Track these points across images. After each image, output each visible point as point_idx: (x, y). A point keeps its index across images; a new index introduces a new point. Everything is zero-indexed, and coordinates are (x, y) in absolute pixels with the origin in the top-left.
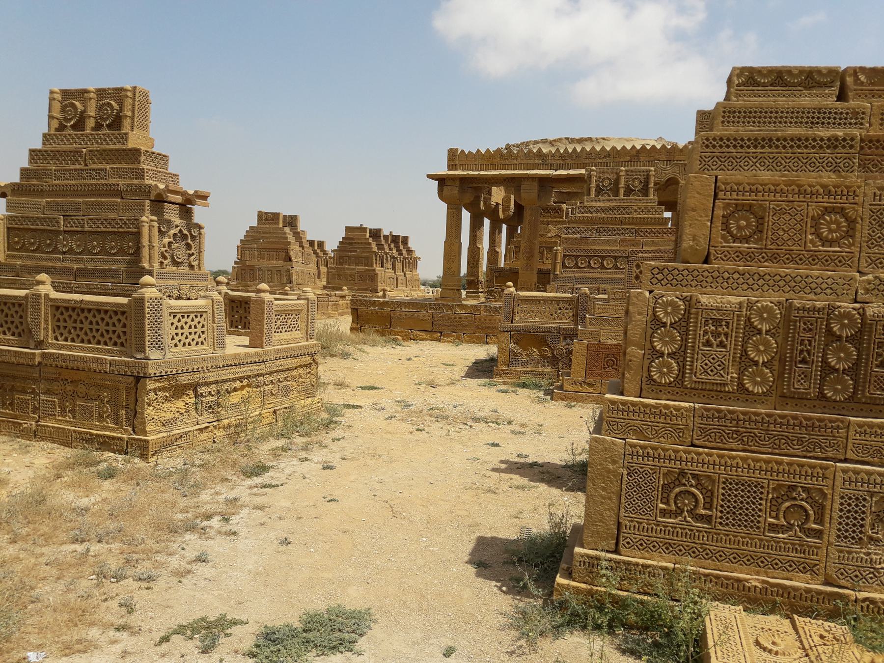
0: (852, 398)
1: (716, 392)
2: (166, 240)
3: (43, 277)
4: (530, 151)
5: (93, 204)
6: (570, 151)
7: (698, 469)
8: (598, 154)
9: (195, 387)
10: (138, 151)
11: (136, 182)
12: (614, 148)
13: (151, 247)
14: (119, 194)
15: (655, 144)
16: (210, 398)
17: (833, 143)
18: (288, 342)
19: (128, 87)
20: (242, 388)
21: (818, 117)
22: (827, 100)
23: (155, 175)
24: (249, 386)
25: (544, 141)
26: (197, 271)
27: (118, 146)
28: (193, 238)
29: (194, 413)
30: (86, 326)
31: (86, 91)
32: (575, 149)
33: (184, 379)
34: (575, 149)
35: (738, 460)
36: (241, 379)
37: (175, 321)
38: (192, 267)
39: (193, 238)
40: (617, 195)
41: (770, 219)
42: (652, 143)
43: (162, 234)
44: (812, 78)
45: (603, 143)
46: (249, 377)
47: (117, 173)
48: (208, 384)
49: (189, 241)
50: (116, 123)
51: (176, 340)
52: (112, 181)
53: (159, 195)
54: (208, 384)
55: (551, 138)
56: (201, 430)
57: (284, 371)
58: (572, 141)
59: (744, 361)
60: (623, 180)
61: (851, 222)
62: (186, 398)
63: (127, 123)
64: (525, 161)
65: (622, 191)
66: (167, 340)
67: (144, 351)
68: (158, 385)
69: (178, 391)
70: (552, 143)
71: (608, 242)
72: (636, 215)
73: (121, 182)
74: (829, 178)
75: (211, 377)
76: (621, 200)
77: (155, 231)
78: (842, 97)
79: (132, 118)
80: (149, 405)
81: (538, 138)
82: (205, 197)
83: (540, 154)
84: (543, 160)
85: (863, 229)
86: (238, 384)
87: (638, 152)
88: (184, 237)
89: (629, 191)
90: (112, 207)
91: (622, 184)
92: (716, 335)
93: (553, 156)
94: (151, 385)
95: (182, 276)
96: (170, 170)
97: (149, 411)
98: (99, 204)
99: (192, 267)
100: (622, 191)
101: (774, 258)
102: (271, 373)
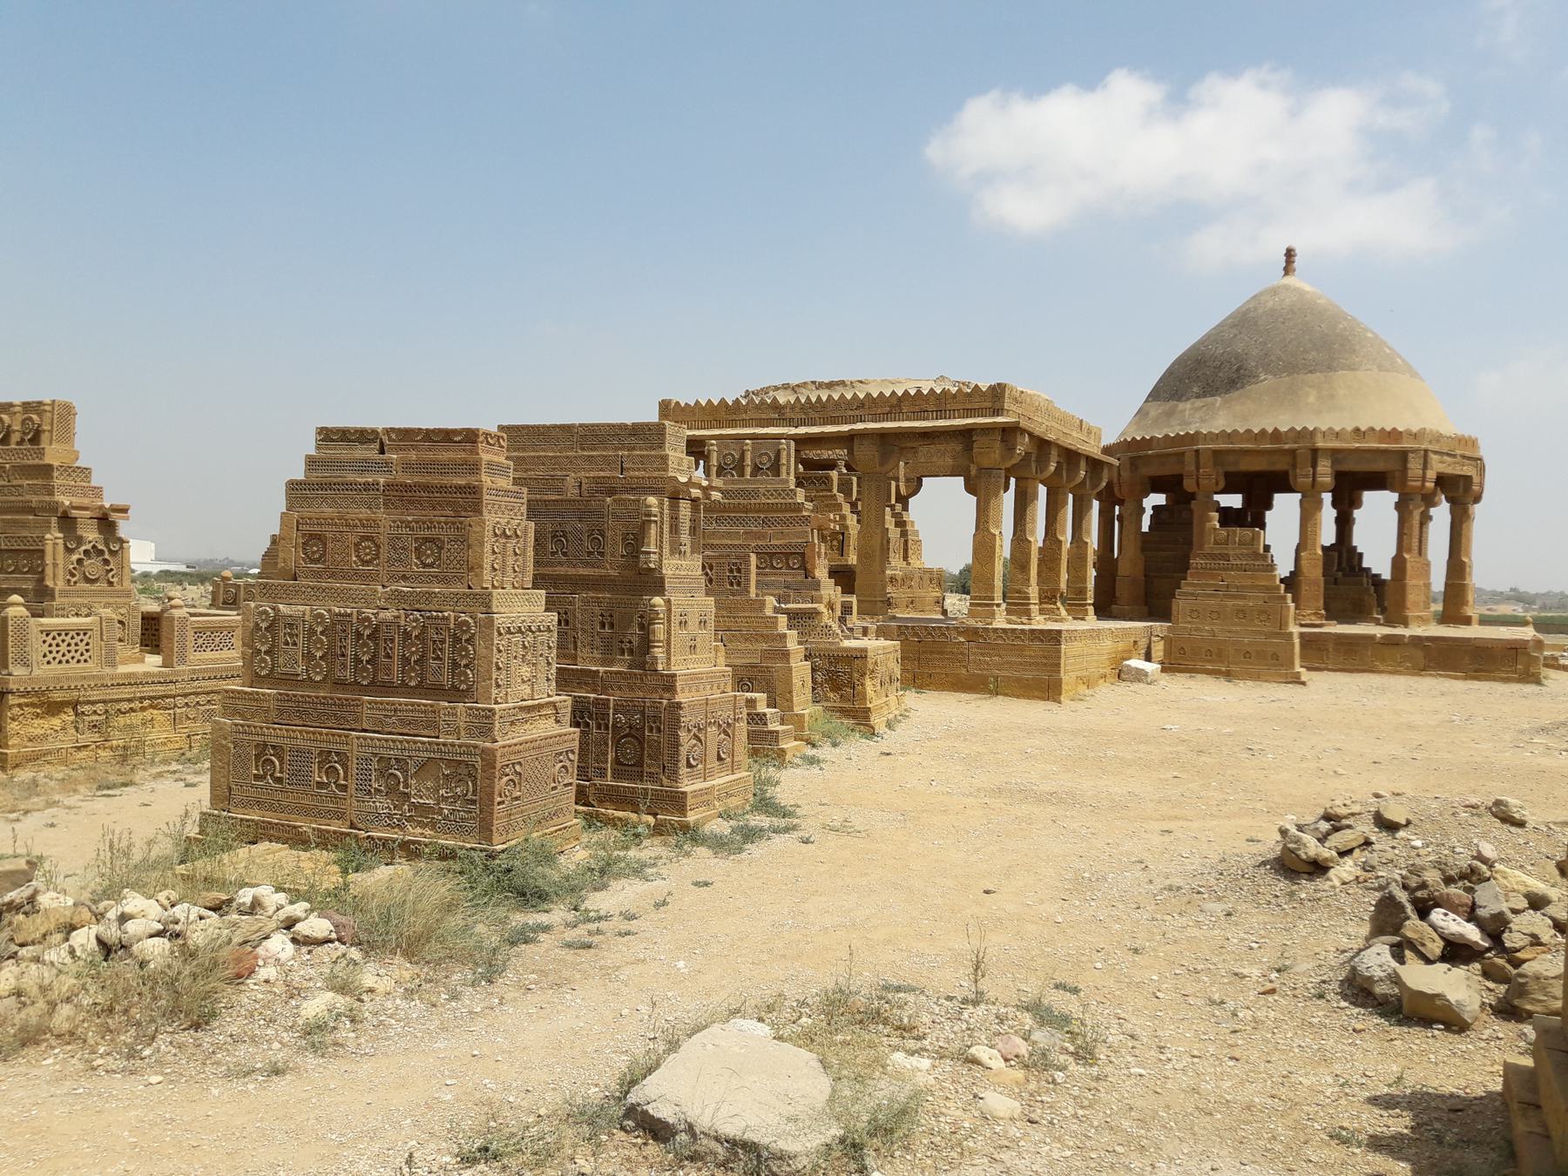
0: (372, 683)
1: (290, 680)
2: (75, 557)
3: (16, 598)
4: (763, 402)
5: (8, 521)
6: (814, 400)
7: (274, 741)
8: (849, 403)
9: (75, 705)
10: (50, 467)
11: (47, 498)
12: (868, 395)
13: (55, 565)
14: (32, 511)
15: (933, 385)
16: (95, 718)
17: (367, 487)
18: (214, 661)
19: (47, 401)
20: (143, 709)
21: (365, 466)
22: (371, 452)
23: (69, 491)
24: (154, 707)
25: (786, 387)
26: (118, 587)
27: (36, 462)
28: (113, 553)
29: (73, 731)
30: (63, 647)
31: (11, 405)
32: (819, 398)
33: (58, 696)
34: (819, 398)
35: (296, 736)
36: (142, 699)
37: (49, 639)
38: (111, 584)
39: (113, 553)
40: (742, 474)
41: (330, 545)
42: (932, 385)
43: (69, 551)
44: (363, 436)
45: (840, 390)
46: (150, 698)
47: (33, 490)
48: (93, 703)
49: (107, 556)
50: (35, 440)
51: (50, 657)
52: (28, 497)
53: (65, 512)
54: (93, 703)
55: (794, 381)
56: (79, 748)
57: (208, 693)
58: (820, 386)
59: (309, 656)
60: (748, 456)
61: (378, 547)
62: (64, 716)
63: (45, 437)
64: (757, 416)
65: (748, 470)
66: (36, 657)
67: (6, 667)
68: (22, 700)
69: (53, 708)
70: (794, 389)
71: (729, 535)
72: (764, 500)
73: (35, 498)
74: (364, 513)
75: (95, 695)
76: (748, 481)
77: (61, 548)
78: (382, 452)
79: (51, 431)
80: (13, 719)
81: (778, 383)
82: (124, 510)
83: (775, 405)
84: (779, 413)
85: (384, 555)
86: (125, 706)
87: (899, 399)
88: (101, 552)
89: (757, 470)
90: (24, 525)
91: (748, 461)
92: (291, 635)
93: (793, 407)
94: (12, 700)
95: (100, 593)
96: (93, 484)
97: (13, 727)
98: (15, 521)
99: (111, 584)
100: (748, 470)
101: (333, 575)
102: (185, 695)
